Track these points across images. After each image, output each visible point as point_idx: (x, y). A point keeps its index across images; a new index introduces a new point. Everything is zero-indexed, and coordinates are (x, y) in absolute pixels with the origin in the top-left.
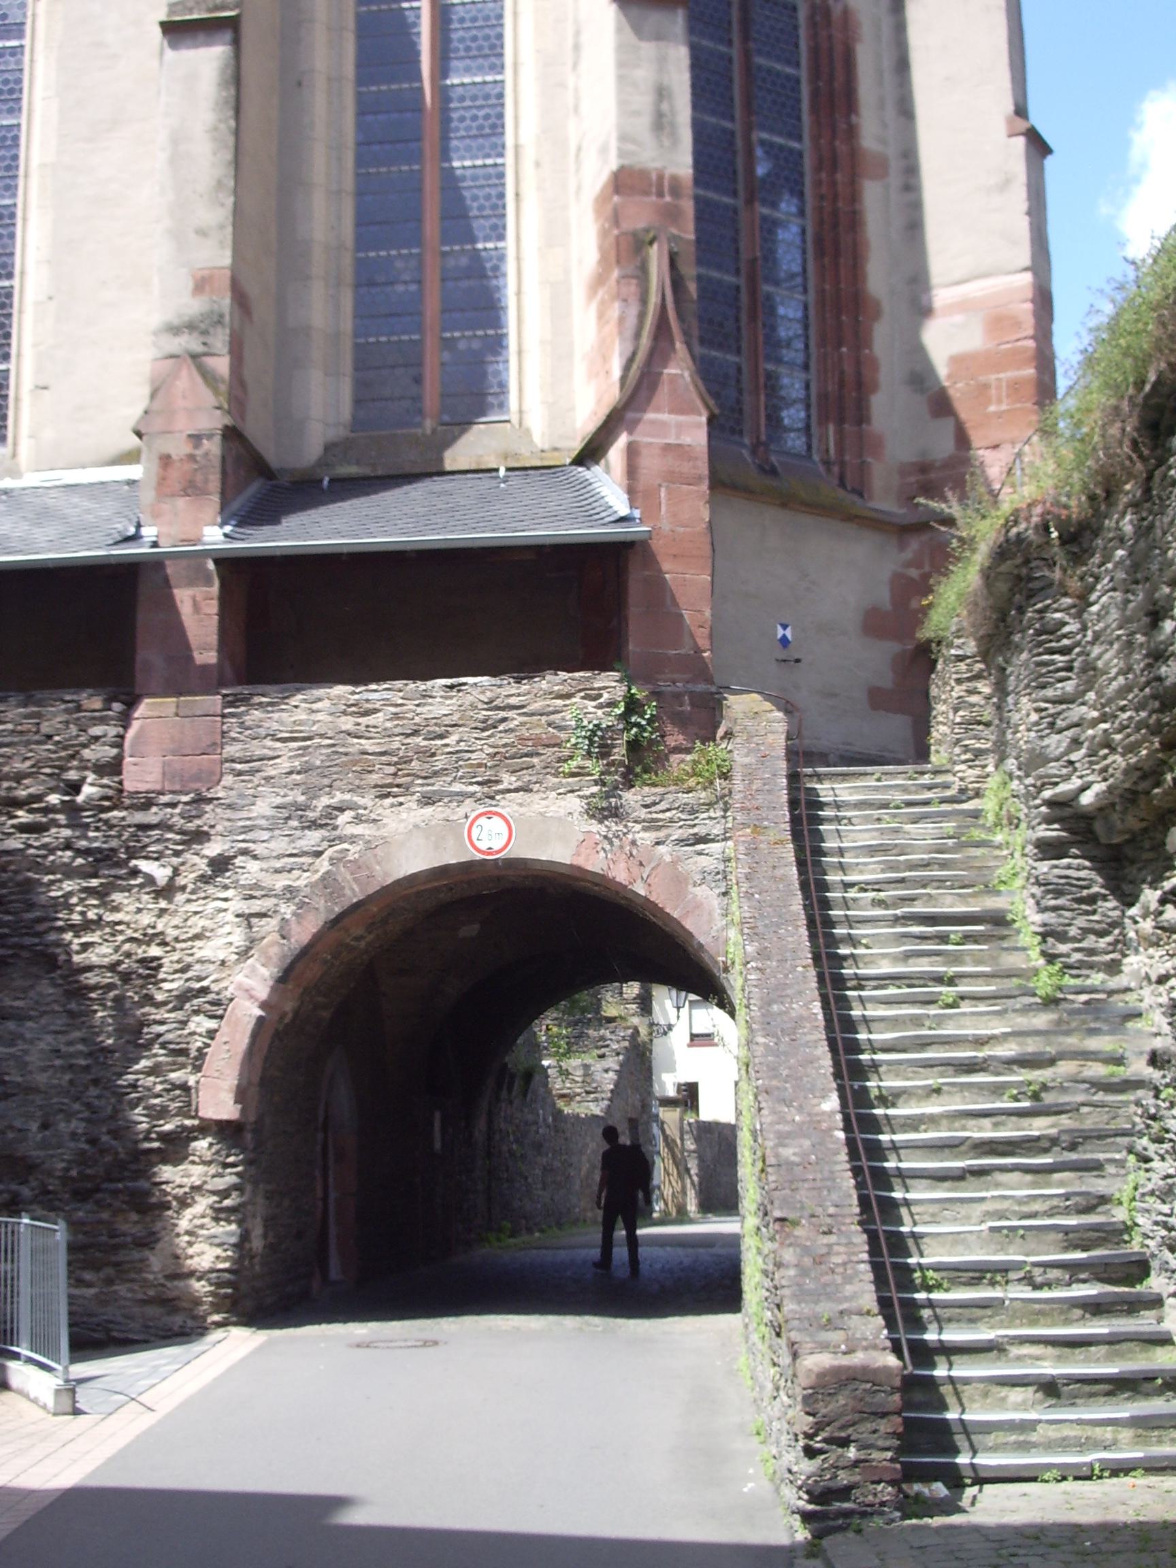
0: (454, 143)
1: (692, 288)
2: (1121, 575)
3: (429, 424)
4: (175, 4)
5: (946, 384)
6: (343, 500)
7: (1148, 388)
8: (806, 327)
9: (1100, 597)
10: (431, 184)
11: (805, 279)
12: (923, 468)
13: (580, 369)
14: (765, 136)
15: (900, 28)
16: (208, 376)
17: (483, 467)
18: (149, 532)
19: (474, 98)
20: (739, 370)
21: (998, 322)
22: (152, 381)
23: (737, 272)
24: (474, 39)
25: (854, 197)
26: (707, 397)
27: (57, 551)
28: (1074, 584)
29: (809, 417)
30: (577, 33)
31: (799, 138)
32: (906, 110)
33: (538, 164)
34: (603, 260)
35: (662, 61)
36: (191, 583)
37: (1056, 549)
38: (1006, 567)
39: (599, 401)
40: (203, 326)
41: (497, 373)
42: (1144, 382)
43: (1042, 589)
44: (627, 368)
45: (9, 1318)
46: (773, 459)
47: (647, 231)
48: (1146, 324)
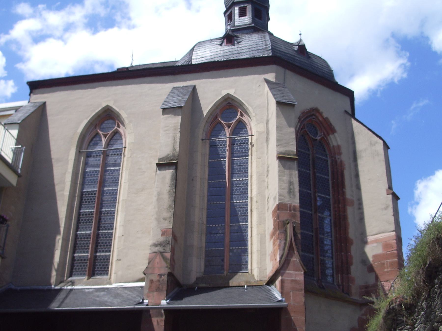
0: (234, 196)
1: (299, 236)
2: (423, 319)
3: (225, 273)
4: (160, 159)
5: (372, 263)
6: (201, 294)
7: (427, 266)
8: (332, 247)
9: (417, 326)
10: (228, 206)
11: (331, 234)
12: (367, 287)
13: (268, 258)
14: (319, 194)
15: (356, 166)
16: (164, 258)
17: (241, 285)
18: (146, 301)
19: (240, 184)
20: (313, 259)
21: (386, 246)
22: (149, 259)
23: (312, 232)
24: (240, 168)
25: (345, 211)
26: (304, 267)
27: (120, 306)
28: (410, 322)
29: (333, 272)
30: (268, 167)
31: (329, 195)
32: (358, 188)
33: (257, 202)
34: (274, 228)
35: (291, 175)
36: (157, 316)
37: (404, 311)
38: (390, 316)
39: (273, 267)
40: (164, 244)
41: (245, 259)
42: (426, 264)
43: (401, 323)
44: (281, 258)
45: (292, 57)
46: (323, 284)
47: (287, 220)
48: (425, 248)
